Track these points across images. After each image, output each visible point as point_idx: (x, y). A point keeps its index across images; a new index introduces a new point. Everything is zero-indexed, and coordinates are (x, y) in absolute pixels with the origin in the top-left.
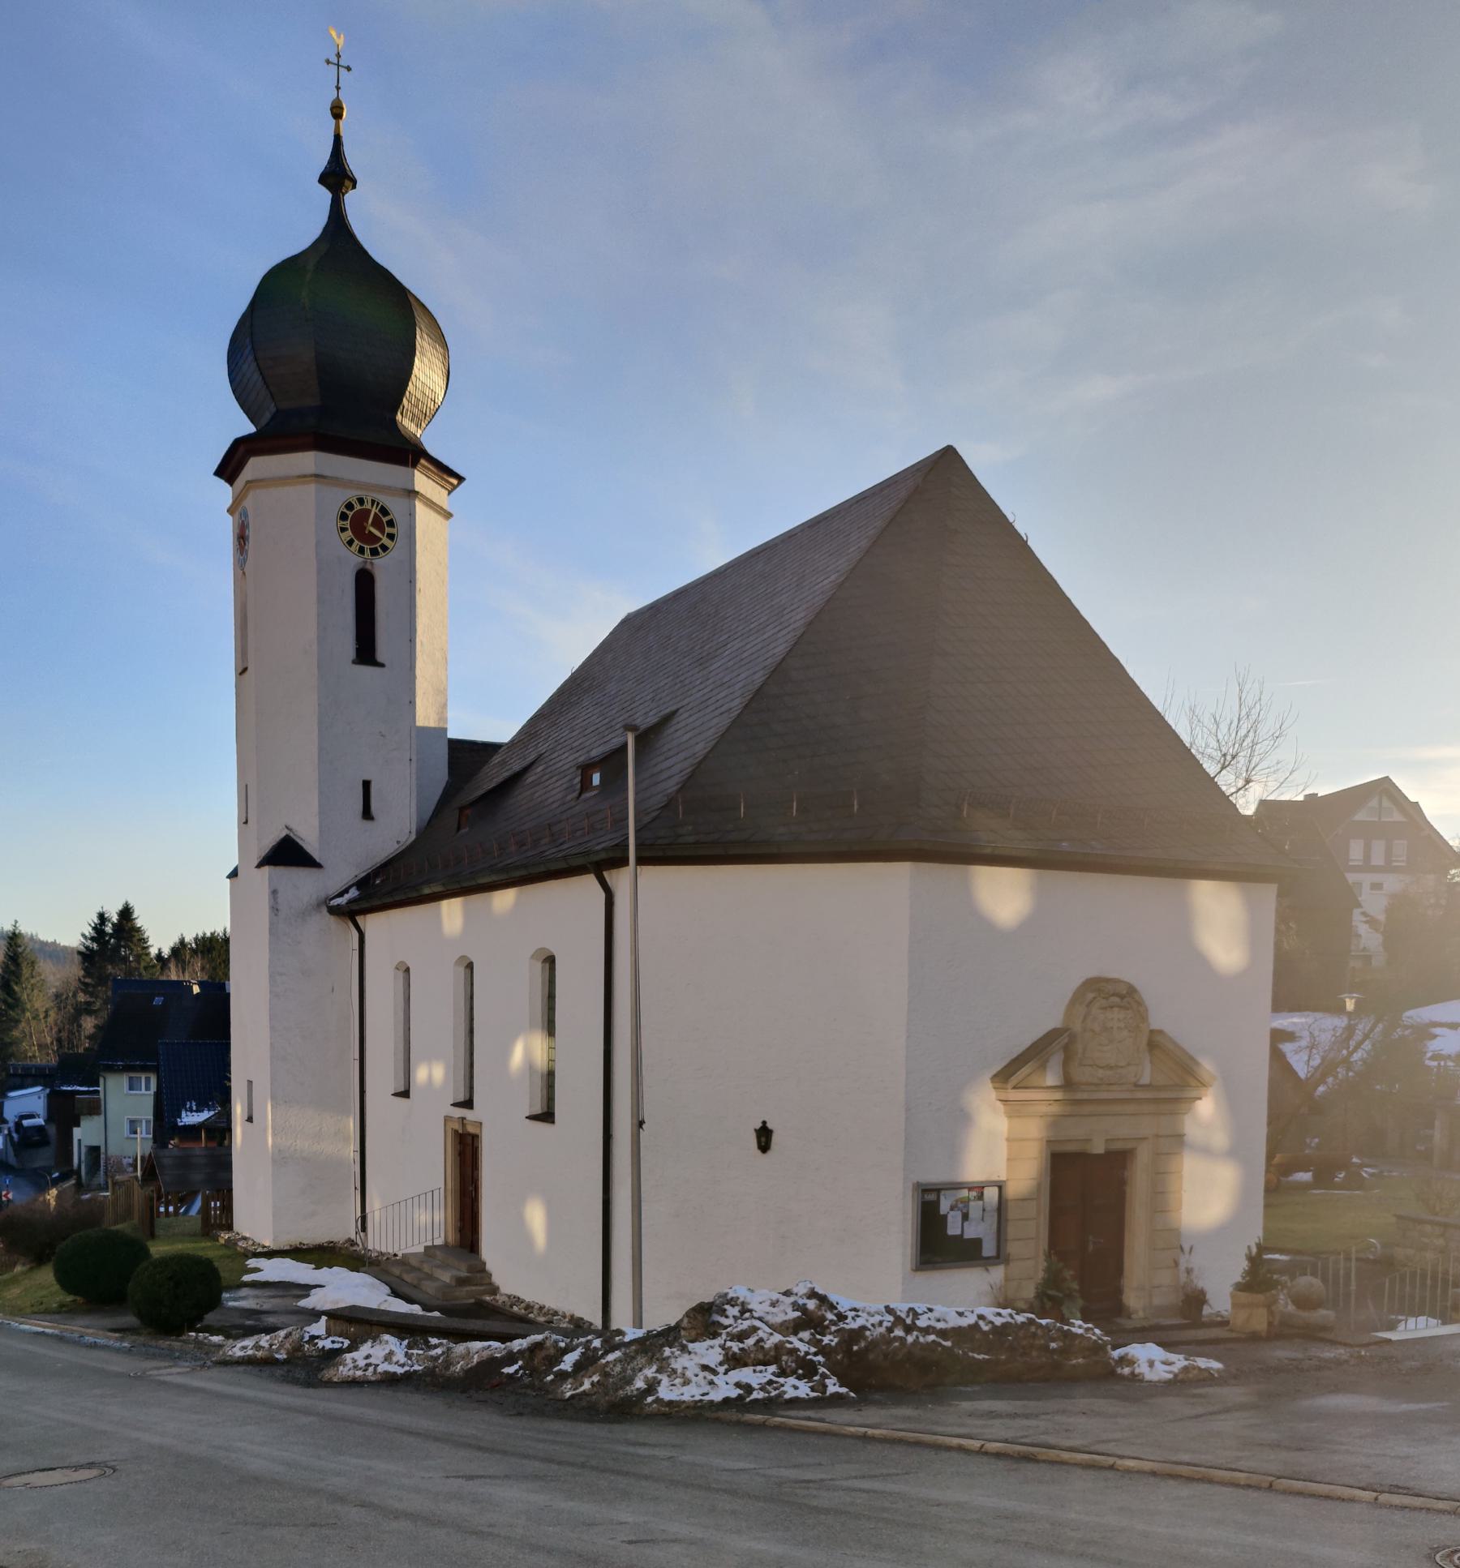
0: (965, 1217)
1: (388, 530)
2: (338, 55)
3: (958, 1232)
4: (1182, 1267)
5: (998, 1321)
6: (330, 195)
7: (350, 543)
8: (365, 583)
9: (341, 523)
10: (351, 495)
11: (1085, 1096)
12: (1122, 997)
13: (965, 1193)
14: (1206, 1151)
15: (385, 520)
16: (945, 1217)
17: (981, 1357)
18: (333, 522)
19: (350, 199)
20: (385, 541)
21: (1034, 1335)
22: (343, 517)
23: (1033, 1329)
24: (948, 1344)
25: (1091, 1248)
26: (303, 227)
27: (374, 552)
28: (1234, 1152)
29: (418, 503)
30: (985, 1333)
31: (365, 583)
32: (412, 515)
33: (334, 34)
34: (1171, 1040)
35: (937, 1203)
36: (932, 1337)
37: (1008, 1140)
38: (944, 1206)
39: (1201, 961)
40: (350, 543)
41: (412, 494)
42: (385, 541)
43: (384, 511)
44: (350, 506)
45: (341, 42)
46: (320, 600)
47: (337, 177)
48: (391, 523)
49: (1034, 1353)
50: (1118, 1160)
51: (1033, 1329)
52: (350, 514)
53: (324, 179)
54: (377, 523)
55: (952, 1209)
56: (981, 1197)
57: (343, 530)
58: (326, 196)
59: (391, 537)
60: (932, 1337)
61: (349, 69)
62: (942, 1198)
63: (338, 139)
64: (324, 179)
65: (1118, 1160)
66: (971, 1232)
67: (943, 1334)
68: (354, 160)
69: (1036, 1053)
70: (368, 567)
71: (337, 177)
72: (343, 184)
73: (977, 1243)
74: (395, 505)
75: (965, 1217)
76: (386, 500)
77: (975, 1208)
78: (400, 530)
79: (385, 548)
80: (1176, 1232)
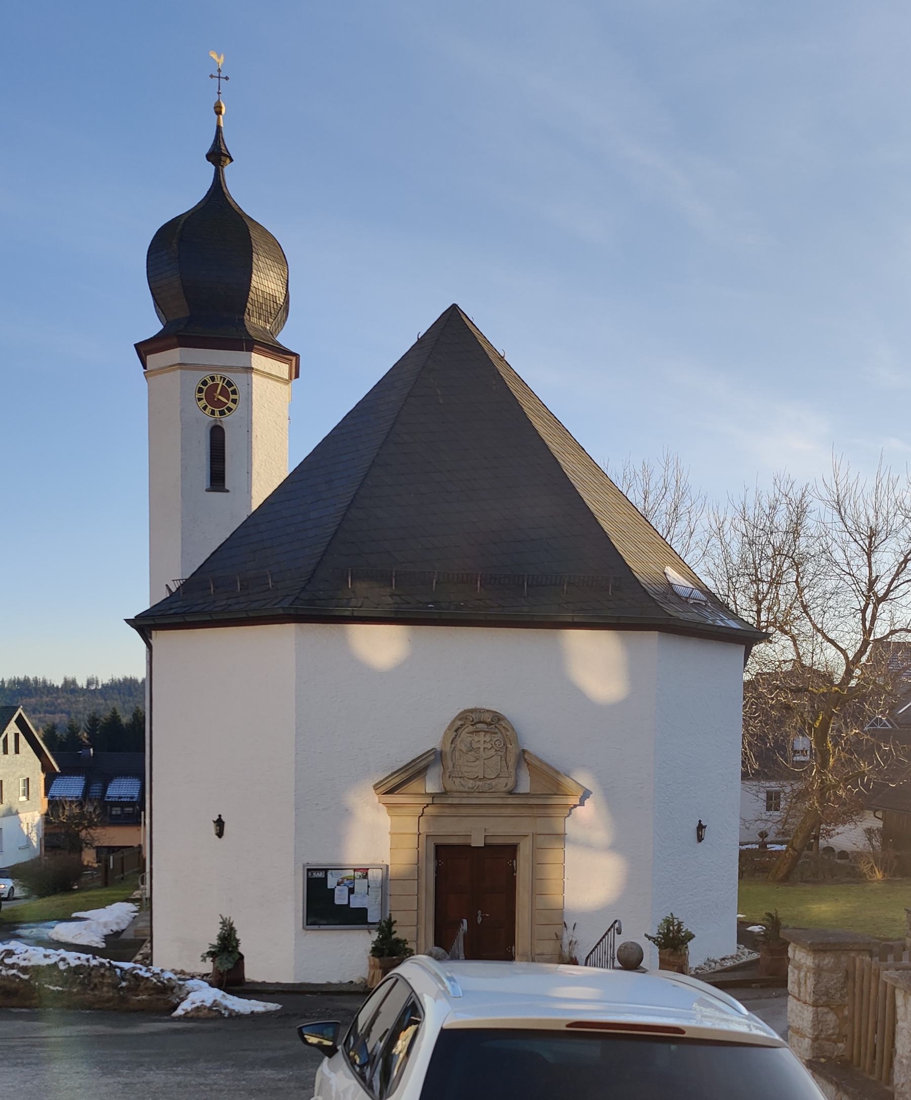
0: (351, 891)
1: (232, 397)
2: (219, 70)
3: (346, 902)
4: (566, 941)
5: (74, 963)
6: (214, 167)
7: (205, 408)
8: (217, 437)
9: (198, 395)
10: (206, 375)
11: (456, 801)
12: (489, 724)
13: (351, 873)
14: (588, 846)
15: (230, 390)
16: (333, 890)
17: (51, 988)
18: (193, 394)
19: (229, 171)
20: (230, 404)
21: (103, 975)
22: (200, 390)
23: (102, 971)
24: (26, 977)
25: (479, 920)
26: (188, 195)
27: (222, 413)
28: (615, 847)
29: (253, 375)
30: (61, 971)
31: (217, 437)
32: (249, 384)
33: (214, 56)
34: (536, 758)
35: (325, 879)
36: (14, 971)
37: (390, 833)
38: (331, 883)
39: (577, 694)
40: (205, 408)
41: (249, 370)
42: (230, 404)
43: (230, 384)
44: (205, 383)
45: (221, 61)
46: (183, 449)
47: (218, 155)
48: (234, 392)
49: (105, 989)
50: (502, 856)
51: (102, 971)
52: (205, 388)
53: (209, 157)
54: (224, 393)
55: (338, 884)
56: (365, 876)
57: (200, 399)
58: (212, 168)
59: (234, 401)
60: (14, 971)
61: (227, 78)
62: (329, 876)
63: (219, 128)
64: (209, 157)
65: (502, 856)
66: (356, 903)
67: (24, 970)
68: (231, 144)
69: (415, 771)
70: (219, 424)
71: (218, 155)
72: (220, 160)
73: (363, 912)
74: (237, 379)
75: (351, 891)
76: (230, 376)
77: (360, 886)
78: (240, 396)
79: (229, 409)
80: (561, 911)
